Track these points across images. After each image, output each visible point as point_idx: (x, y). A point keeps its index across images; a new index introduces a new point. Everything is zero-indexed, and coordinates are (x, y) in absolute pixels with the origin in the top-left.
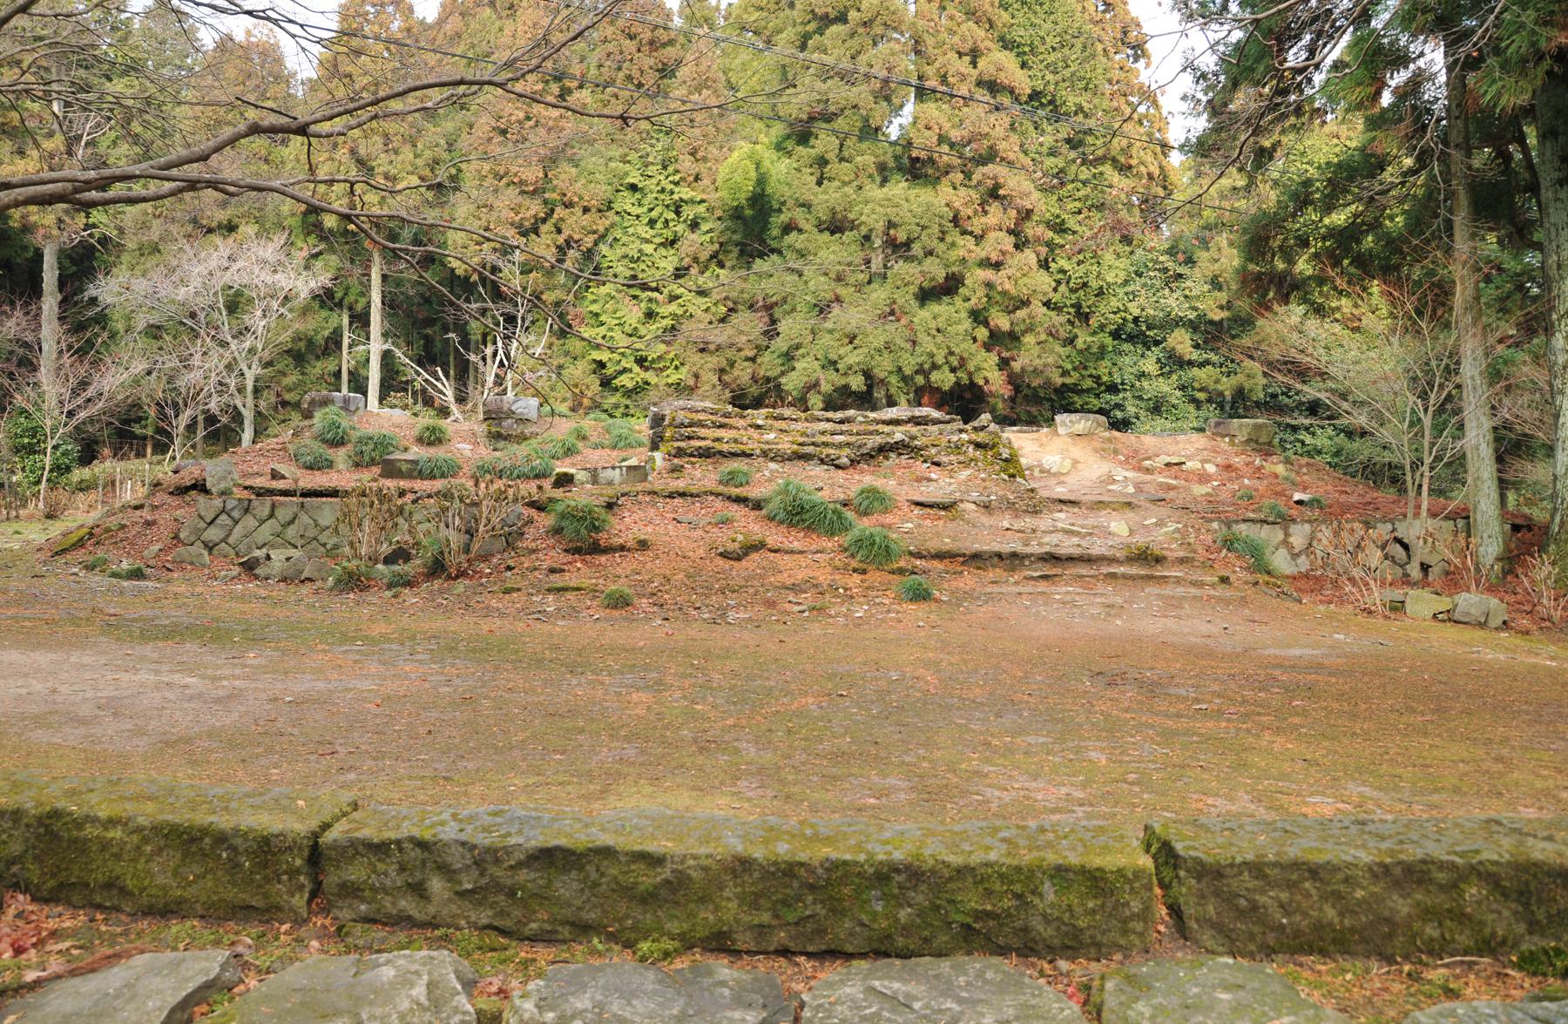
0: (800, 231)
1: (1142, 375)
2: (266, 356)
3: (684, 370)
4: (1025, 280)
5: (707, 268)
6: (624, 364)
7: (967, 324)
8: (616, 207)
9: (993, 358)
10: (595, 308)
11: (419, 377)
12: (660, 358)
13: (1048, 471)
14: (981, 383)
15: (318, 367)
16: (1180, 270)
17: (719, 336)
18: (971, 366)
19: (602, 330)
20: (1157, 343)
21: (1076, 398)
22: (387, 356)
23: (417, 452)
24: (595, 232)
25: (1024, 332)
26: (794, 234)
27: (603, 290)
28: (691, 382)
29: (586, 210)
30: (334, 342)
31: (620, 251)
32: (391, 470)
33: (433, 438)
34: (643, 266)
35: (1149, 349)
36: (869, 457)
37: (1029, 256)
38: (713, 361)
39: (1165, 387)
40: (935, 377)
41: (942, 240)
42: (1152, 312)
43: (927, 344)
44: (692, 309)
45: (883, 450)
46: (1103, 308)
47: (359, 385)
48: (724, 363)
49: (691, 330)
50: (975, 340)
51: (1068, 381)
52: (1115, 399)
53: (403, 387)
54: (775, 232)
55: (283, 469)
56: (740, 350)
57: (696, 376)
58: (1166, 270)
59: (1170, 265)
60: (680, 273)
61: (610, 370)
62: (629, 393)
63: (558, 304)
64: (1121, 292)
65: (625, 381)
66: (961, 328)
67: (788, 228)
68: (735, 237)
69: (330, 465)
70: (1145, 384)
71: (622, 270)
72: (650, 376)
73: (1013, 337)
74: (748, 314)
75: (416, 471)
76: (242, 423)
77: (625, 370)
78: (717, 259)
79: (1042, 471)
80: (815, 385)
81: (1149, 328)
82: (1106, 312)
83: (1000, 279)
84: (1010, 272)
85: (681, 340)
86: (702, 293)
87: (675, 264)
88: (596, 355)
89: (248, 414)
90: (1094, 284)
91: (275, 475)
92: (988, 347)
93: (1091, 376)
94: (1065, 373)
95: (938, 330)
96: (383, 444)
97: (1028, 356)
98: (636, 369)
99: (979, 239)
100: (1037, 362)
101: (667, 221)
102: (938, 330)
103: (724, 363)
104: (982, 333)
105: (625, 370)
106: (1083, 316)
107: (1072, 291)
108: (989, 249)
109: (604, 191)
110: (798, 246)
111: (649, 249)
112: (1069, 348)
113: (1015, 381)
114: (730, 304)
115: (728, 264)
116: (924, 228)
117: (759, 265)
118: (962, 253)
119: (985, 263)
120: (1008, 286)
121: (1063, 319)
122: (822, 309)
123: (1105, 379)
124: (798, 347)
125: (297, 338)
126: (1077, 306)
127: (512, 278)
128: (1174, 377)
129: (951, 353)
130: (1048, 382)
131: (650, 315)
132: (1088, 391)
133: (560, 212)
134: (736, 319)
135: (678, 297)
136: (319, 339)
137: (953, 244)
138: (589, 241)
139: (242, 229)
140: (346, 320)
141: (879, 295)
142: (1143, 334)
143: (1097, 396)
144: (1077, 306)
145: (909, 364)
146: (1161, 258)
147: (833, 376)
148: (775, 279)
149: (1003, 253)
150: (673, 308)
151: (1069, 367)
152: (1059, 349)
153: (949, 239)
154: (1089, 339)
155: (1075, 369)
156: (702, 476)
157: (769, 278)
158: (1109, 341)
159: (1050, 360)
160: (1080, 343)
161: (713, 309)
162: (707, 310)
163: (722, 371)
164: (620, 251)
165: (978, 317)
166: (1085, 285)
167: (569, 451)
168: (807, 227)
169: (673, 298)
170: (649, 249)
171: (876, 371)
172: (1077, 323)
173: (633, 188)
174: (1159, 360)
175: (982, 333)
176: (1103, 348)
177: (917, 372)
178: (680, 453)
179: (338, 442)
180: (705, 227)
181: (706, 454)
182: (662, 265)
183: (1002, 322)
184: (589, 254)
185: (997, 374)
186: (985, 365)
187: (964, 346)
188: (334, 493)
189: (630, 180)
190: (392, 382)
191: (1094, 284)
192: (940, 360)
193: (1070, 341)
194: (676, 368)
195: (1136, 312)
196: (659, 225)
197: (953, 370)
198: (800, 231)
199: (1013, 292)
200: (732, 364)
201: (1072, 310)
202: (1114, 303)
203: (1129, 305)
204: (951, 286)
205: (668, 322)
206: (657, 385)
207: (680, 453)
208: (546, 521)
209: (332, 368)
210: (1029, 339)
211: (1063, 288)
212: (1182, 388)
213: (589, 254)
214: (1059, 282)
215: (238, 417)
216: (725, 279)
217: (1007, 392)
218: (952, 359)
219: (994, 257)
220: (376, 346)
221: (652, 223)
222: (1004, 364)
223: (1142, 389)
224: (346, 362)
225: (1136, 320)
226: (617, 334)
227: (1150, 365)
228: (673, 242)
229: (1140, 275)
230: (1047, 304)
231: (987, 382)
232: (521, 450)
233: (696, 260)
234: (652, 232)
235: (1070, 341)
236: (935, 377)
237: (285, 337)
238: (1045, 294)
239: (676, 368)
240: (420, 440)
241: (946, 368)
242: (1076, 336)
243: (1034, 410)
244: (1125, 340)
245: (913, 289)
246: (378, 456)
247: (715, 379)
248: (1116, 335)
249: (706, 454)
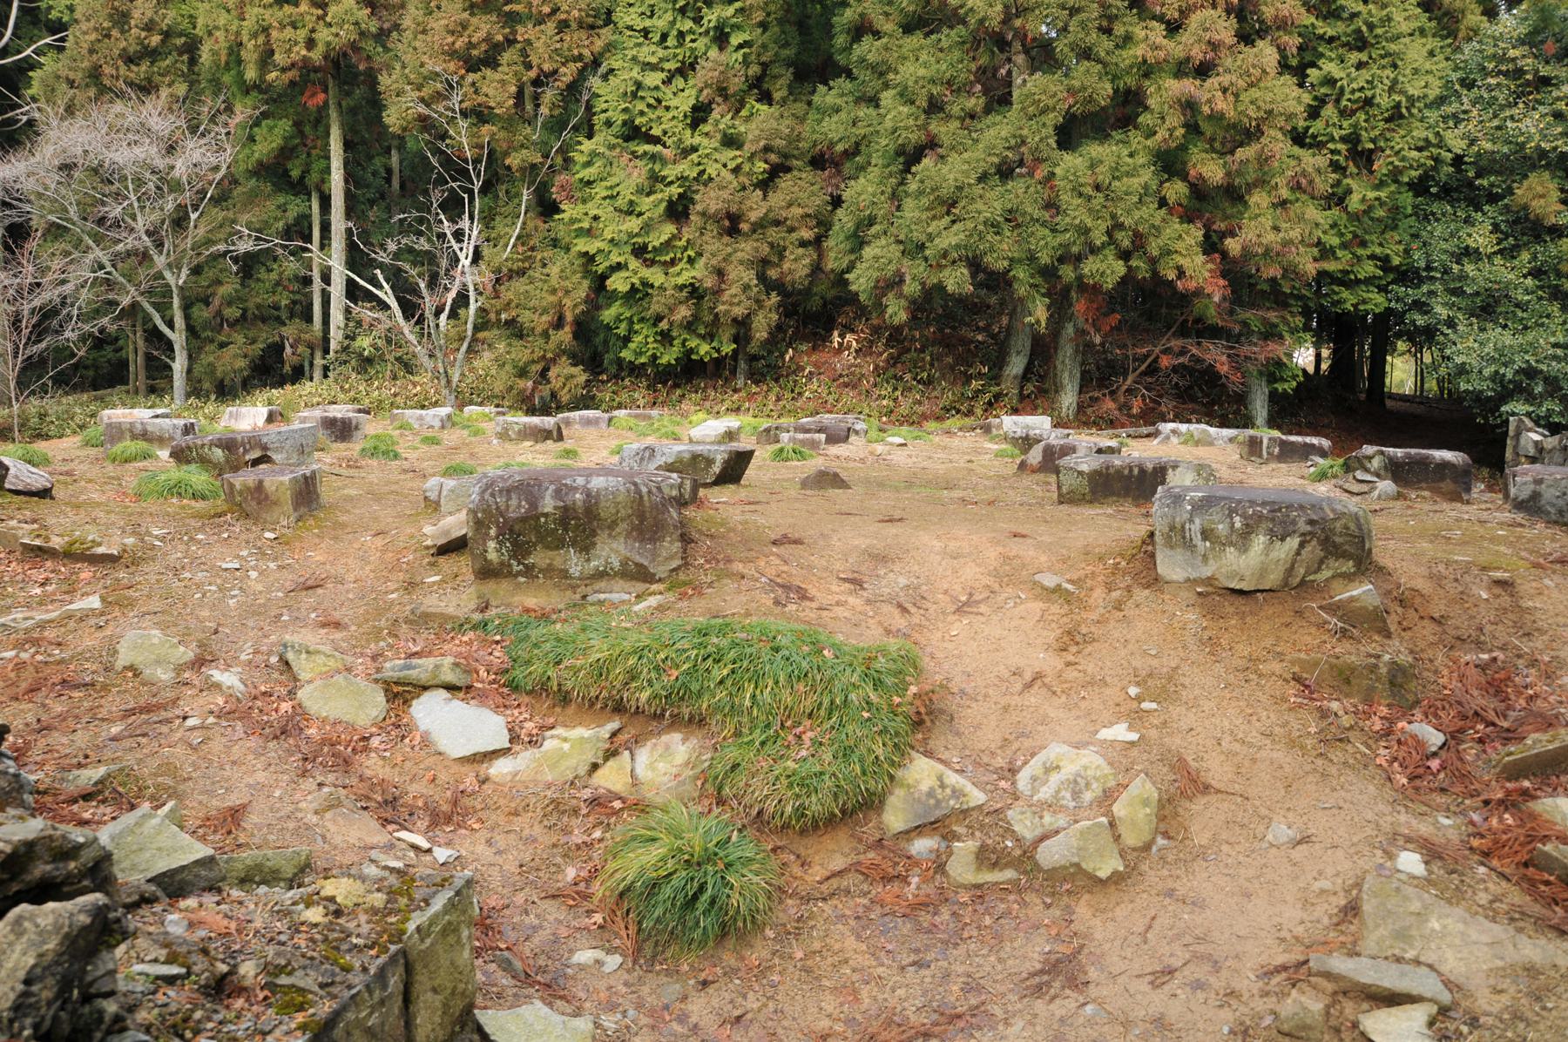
0: (877, 34)
1: (1468, 253)
3: (701, 262)
4: (1254, 93)
5: (742, 104)
7: (1147, 176)
9: (1196, 233)
12: (668, 245)
13: (1025, 858)
14: (1171, 275)
16: (1545, 71)
17: (756, 207)
18: (1154, 248)
20: (1493, 199)
21: (1345, 294)
24: (580, 58)
25: (1250, 187)
26: (867, 40)
29: (563, 26)
34: (641, 106)
35: (1478, 208)
37: (1266, 53)
38: (747, 248)
39: (1508, 274)
40: (1090, 266)
41: (1108, 31)
42: (1488, 146)
43: (1076, 212)
46: (1398, 142)
48: (765, 250)
50: (1163, 203)
51: (1331, 266)
52: (1412, 294)
54: (840, 40)
56: (791, 230)
57: (720, 273)
58: (1519, 72)
59: (1528, 63)
60: (699, 115)
64: (1433, 115)
66: (1135, 183)
67: (861, 30)
68: (786, 52)
70: (1469, 268)
72: (656, 276)
73: (1234, 194)
74: (808, 175)
76: (173, 350)
77: (619, 267)
78: (760, 88)
79: (987, 857)
80: (897, 281)
81: (1479, 175)
82: (1403, 149)
83: (1207, 93)
84: (1226, 79)
86: (731, 141)
87: (692, 101)
90: (1384, 101)
92: (1188, 217)
93: (1372, 257)
94: (1326, 253)
95: (1098, 188)
97: (1257, 229)
98: (634, 263)
99: (1173, 28)
100: (1270, 238)
101: (681, 35)
102: (1098, 188)
103: (765, 250)
104: (1176, 190)
105: (619, 267)
106: (1363, 158)
107: (1344, 113)
108: (1188, 45)
110: (871, 58)
112: (1335, 211)
113: (1237, 275)
114: (773, 157)
115: (777, 96)
116: (1074, 11)
117: (825, 96)
118: (1139, 51)
119: (1181, 69)
120: (1222, 105)
121: (1322, 161)
122: (910, 157)
123: (1396, 261)
124: (871, 221)
126: (1352, 140)
128: (1525, 256)
129: (1120, 226)
130: (1290, 271)
132: (1369, 281)
134: (785, 182)
135: (694, 149)
137: (1128, 39)
138: (568, 73)
139: (846, 196)
141: (998, 132)
142: (1470, 184)
143: (1383, 289)
144: (1352, 140)
145: (1045, 246)
146: (1512, 53)
147: (920, 268)
148: (843, 115)
149: (1214, 46)
151: (1335, 241)
152: (1313, 212)
153: (1119, 30)
154: (1371, 195)
155: (1344, 246)
157: (833, 116)
158: (1407, 199)
159: (1295, 234)
160: (1354, 203)
161: (746, 168)
162: (736, 170)
163: (765, 262)
165: (1170, 163)
166: (1368, 102)
168: (888, 27)
170: (654, 79)
171: (988, 259)
172: (1352, 169)
174: (1496, 228)
175: (1176, 190)
176: (1395, 210)
177: (1061, 260)
180: (735, 40)
182: (672, 103)
183: (1212, 170)
185: (1200, 259)
186: (1180, 246)
187: (1144, 212)
191: (1384, 101)
192: (1099, 238)
193: (1337, 199)
194: (691, 261)
195: (1458, 146)
196: (671, 42)
197: (1125, 256)
198: (877, 34)
199: (1231, 114)
200: (780, 252)
201: (1341, 147)
202: (1420, 133)
203: (1448, 135)
204: (1126, 109)
205: (675, 190)
206: (662, 288)
210: (1259, 199)
211: (1329, 111)
212: (1536, 273)
214: (1322, 101)
216: (762, 122)
217: (1217, 291)
218: (1119, 235)
219: (1197, 54)
222: (1211, 245)
223: (1463, 277)
225: (1458, 160)
227: (1480, 237)
229: (1468, 84)
230: (1299, 138)
231: (1181, 273)
233: (722, 91)
234: (661, 53)
235: (1337, 199)
236: (1090, 266)
238: (1290, 117)
239: (691, 261)
242: (1349, 191)
243: (1273, 316)
244: (1437, 197)
245: (1053, 119)
247: (749, 276)
248: (1419, 187)
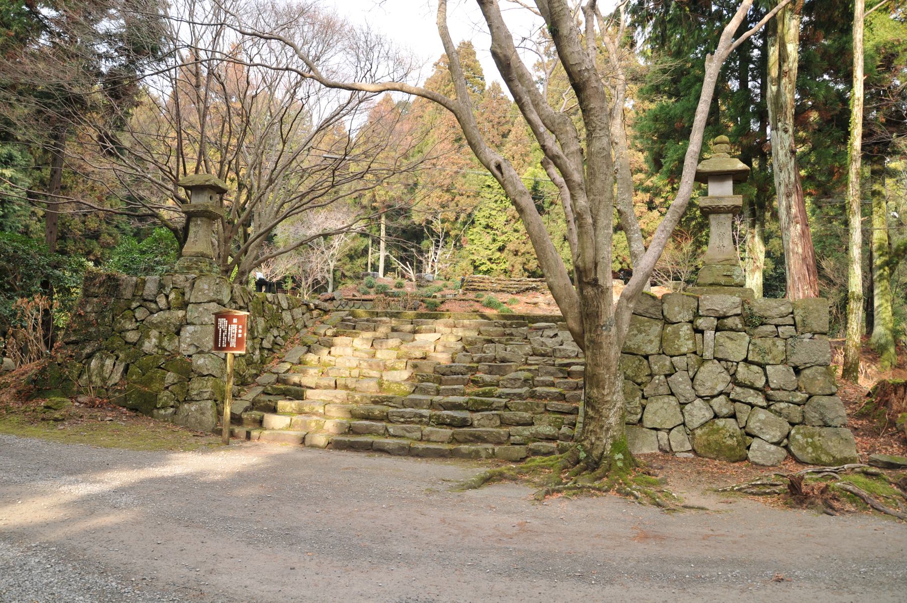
2: (339, 257)
6: (483, 261)
8: (482, 194)
10: (472, 237)
11: (400, 266)
12: (498, 258)
15: (360, 262)
19: (475, 247)
22: (387, 259)
23: (394, 290)
27: (475, 230)
28: (510, 269)
30: (365, 252)
31: (482, 214)
32: (386, 294)
33: (400, 286)
36: (524, 291)
38: (520, 259)
44: (511, 238)
45: (527, 289)
47: (375, 268)
49: (510, 246)
53: (394, 270)
55: (356, 294)
57: (513, 266)
61: (477, 263)
62: (486, 272)
63: (457, 235)
65: (483, 268)
69: (369, 293)
71: (483, 222)
72: (494, 266)
75: (394, 295)
85: (506, 251)
88: (472, 257)
89: (331, 281)
91: (354, 296)
96: (385, 287)
98: (488, 263)
109: (476, 188)
111: (494, 213)
125: (351, 250)
127: (438, 226)
131: (494, 240)
133: (458, 198)
136: (360, 250)
138: (469, 210)
140: (370, 242)
149: (642, 213)
150: (504, 237)
156: (471, 295)
163: (525, 264)
164: (482, 214)
167: (440, 290)
169: (503, 233)
170: (494, 213)
173: (489, 186)
178: (467, 289)
179: (371, 287)
181: (474, 290)
184: (470, 215)
188: (371, 300)
189: (487, 183)
190: (388, 268)
197: (621, 263)
205: (501, 244)
207: (467, 289)
208: (424, 305)
209: (365, 262)
213: (470, 215)
215: (327, 283)
220: (383, 254)
221: (496, 201)
224: (370, 259)
226: (480, 249)
228: (505, 209)
232: (425, 289)
237: (346, 249)
240: (396, 287)
241: (617, 262)
246: (383, 290)
247: (521, 267)
249: (474, 290)
